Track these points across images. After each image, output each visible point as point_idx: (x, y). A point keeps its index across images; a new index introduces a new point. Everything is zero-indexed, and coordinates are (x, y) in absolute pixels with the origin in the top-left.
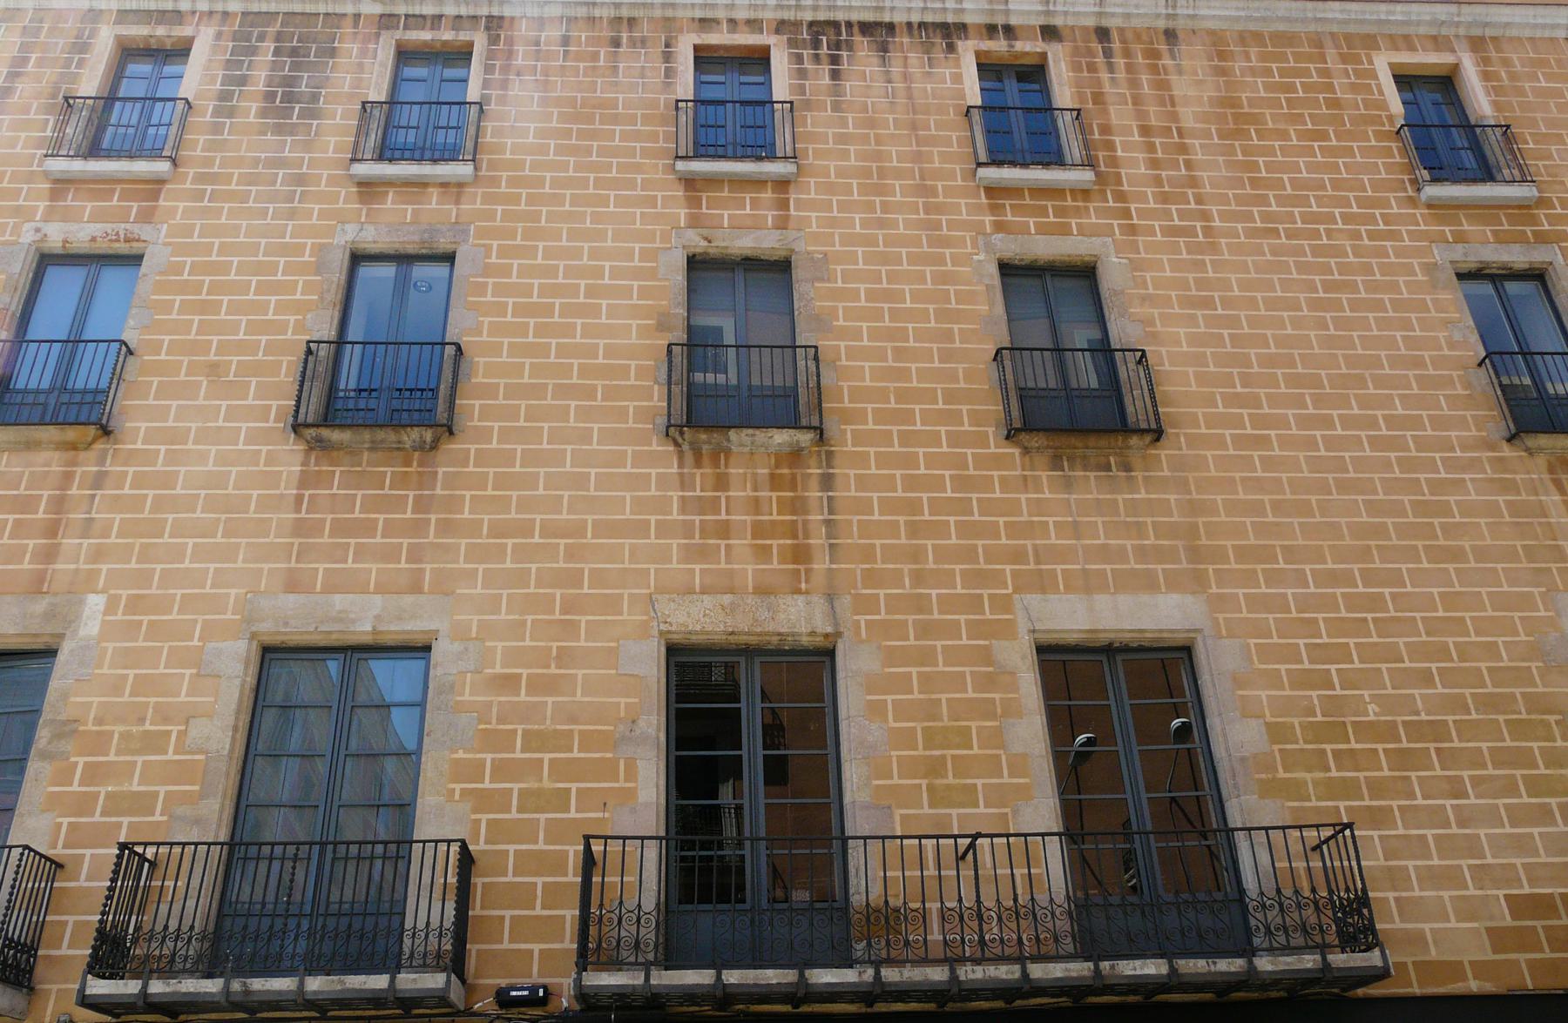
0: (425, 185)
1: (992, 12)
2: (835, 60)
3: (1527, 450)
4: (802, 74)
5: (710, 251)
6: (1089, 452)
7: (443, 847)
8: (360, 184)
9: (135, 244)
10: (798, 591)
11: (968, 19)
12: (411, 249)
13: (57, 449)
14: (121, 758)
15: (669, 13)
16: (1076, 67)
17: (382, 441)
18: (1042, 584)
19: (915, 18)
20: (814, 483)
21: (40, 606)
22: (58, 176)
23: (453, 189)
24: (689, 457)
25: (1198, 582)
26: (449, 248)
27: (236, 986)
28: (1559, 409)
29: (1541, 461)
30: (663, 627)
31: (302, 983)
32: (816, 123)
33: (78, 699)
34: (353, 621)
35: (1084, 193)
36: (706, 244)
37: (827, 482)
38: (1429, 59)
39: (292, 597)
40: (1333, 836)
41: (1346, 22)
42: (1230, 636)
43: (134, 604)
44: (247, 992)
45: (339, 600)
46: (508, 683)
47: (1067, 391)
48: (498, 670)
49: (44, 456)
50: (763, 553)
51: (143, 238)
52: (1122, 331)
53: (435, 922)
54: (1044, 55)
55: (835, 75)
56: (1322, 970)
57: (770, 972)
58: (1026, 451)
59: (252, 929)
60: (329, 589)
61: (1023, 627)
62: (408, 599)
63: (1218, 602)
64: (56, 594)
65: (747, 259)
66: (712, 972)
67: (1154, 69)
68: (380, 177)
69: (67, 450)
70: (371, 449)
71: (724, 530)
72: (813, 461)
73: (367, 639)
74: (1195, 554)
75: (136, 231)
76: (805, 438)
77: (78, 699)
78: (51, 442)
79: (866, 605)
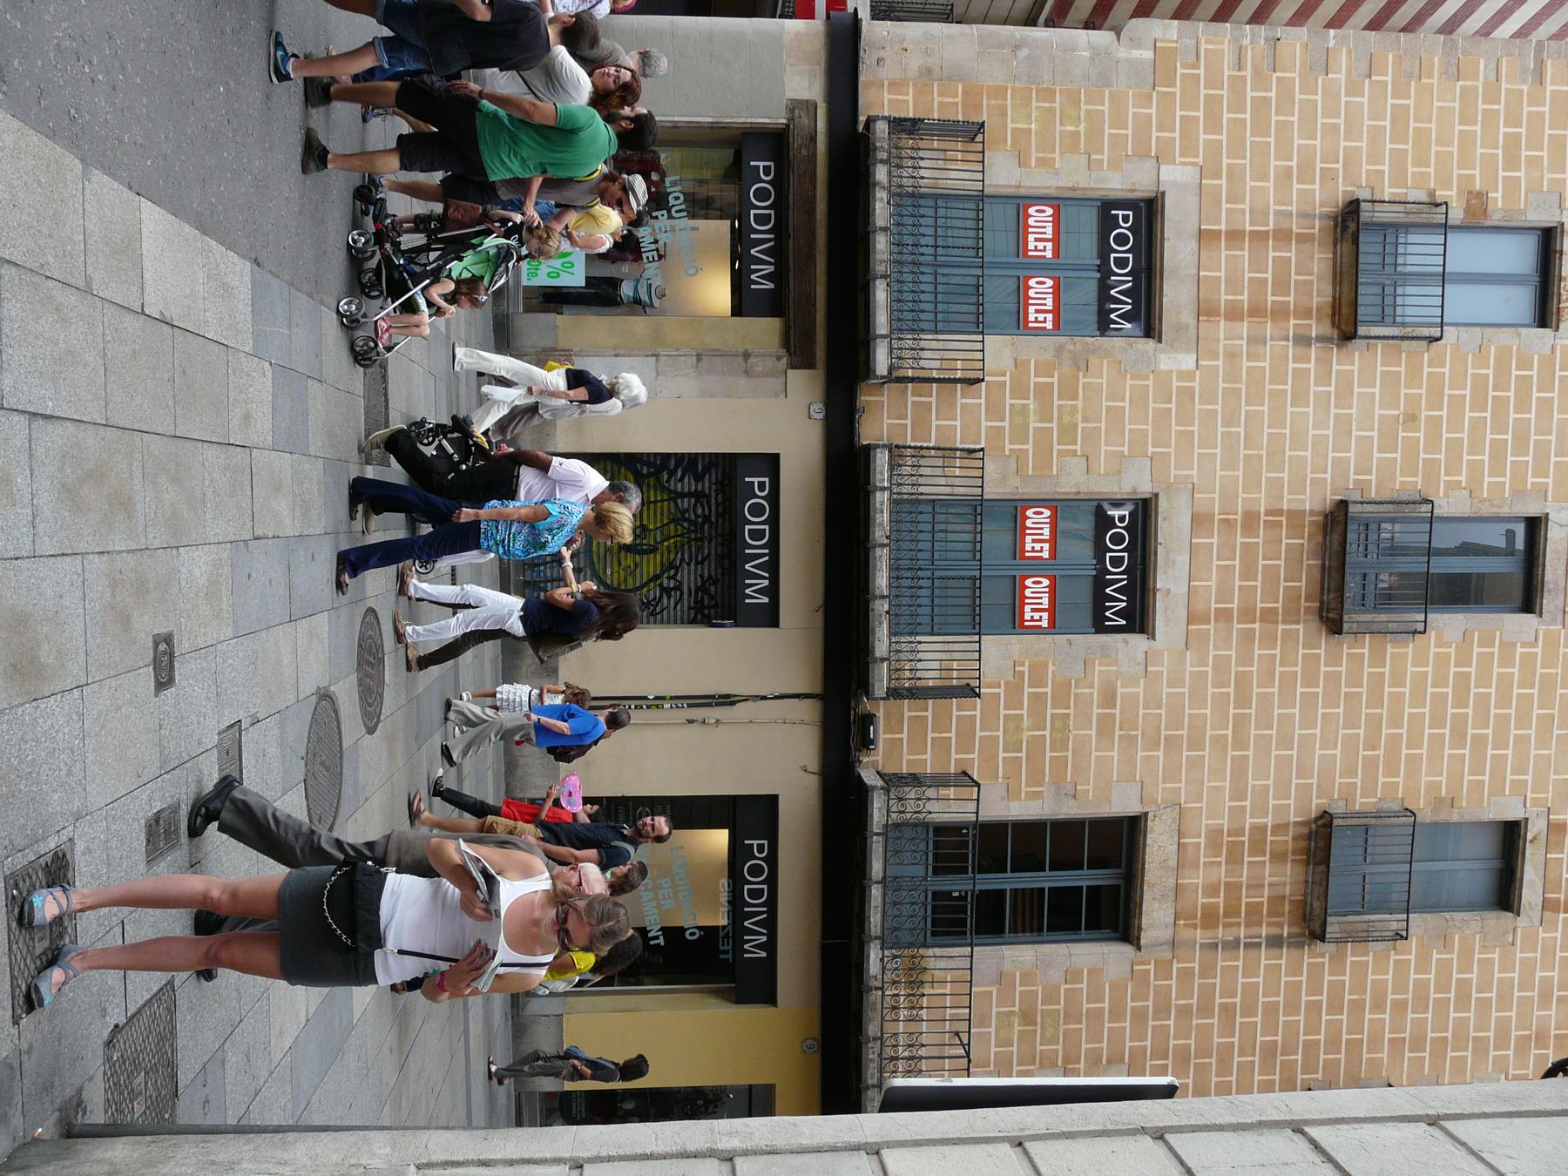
20: (1274, 931)
46: (1109, 698)
48: (1120, 690)
50: (1212, 890)
60: (1192, 548)
71: (1234, 859)
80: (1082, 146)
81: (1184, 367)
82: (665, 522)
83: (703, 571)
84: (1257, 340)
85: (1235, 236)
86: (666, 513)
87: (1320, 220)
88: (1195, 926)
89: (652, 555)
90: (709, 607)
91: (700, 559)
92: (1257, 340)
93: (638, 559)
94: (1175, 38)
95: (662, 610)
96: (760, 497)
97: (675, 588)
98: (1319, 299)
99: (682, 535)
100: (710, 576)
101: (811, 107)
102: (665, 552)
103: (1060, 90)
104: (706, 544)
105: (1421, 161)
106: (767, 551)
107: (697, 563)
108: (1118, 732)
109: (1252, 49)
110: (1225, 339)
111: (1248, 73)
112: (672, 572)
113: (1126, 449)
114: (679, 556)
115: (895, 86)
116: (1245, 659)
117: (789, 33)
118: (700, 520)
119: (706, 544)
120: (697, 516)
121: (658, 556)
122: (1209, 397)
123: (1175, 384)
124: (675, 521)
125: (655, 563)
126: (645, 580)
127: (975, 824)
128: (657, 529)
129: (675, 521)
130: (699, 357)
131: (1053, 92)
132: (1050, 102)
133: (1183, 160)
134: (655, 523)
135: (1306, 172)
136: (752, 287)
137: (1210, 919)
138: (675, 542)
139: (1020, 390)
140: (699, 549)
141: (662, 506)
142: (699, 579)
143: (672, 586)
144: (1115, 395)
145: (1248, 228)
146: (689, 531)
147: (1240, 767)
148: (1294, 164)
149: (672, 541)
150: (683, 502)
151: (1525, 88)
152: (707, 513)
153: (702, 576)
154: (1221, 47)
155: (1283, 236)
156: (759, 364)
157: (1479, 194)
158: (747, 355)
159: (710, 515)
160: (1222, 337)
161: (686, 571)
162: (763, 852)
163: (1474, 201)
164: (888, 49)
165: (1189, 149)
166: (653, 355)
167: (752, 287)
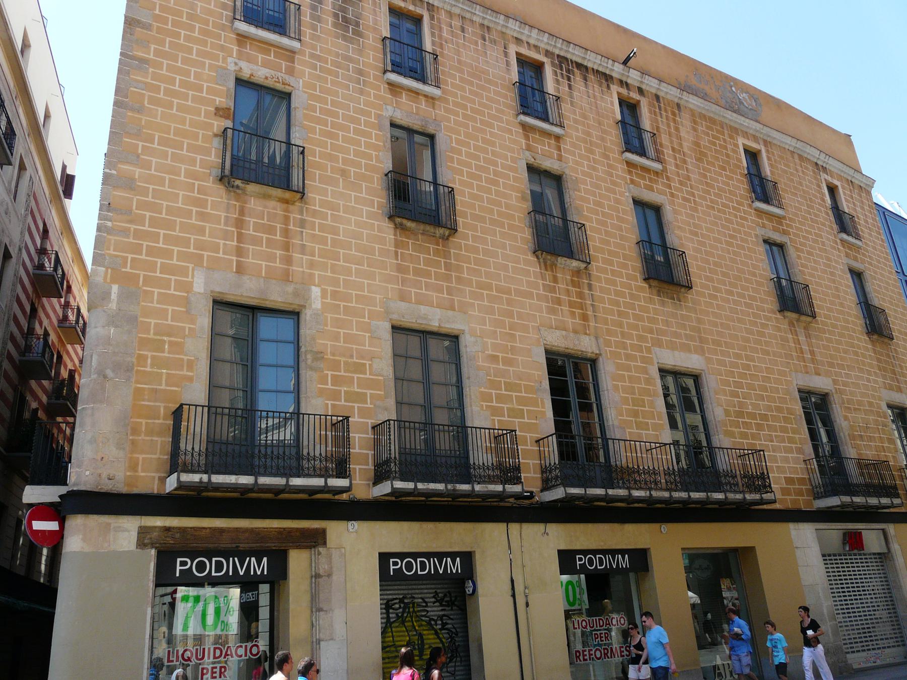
0: (418, 94)
1: (623, 74)
2: (569, 79)
3: (784, 316)
4: (557, 81)
5: (535, 164)
6: (669, 291)
7: (201, 408)
8: (238, 35)
9: (287, 87)
10: (586, 334)
11: (614, 75)
12: (416, 127)
13: (278, 201)
14: (347, 374)
15: (504, 30)
16: (650, 112)
17: (428, 231)
18: (658, 343)
19: (596, 67)
20: (586, 286)
21: (290, 288)
22: (239, 32)
23: (430, 99)
24: (543, 267)
25: (701, 351)
26: (433, 132)
27: (450, 487)
28: (266, 174)
29: (787, 320)
30: (545, 342)
31: (287, 481)
32: (565, 107)
33: (321, 342)
34: (430, 320)
35: (656, 173)
36: (533, 160)
37: (590, 287)
38: (754, 145)
39: (403, 304)
40: (341, 421)
41: (731, 120)
42: (712, 374)
43: (335, 294)
44: (454, 490)
45: (423, 309)
46: (494, 359)
47: (238, 156)
48: (490, 352)
49: (272, 203)
50: (573, 314)
51: (292, 84)
52: (297, 138)
53: (197, 449)
54: (639, 102)
55: (570, 87)
56: (324, 486)
57: (620, 491)
58: (650, 286)
59: (275, 453)
60: (419, 302)
61: (655, 361)
62: (450, 313)
63: (708, 360)
64: (296, 283)
65: (546, 171)
66: (723, 494)
67: (674, 121)
68: (399, 83)
69: (283, 203)
70: (422, 234)
71: (559, 302)
72: (584, 276)
73: (435, 329)
74: (702, 340)
75: (287, 79)
76: (583, 265)
77: (321, 342)
78: (276, 197)
79: (608, 343)
80: (179, 340)
81: (319, 294)
82: (404, 629)
83: (431, 602)
84: (303, 249)
85: (240, 252)
86: (399, 629)
87: (230, 200)
88: (589, 325)
89: (424, 637)
90: (451, 597)
91: (424, 604)
92: (303, 249)
93: (426, 646)
94: (104, 269)
95: (454, 628)
96: (402, 564)
97: (442, 620)
98: (278, 209)
99: (411, 617)
100: (434, 597)
101: (143, 532)
102: (422, 628)
103: (139, 350)
104: (416, 600)
105: (195, 137)
106: (231, 559)
107: (427, 606)
108: (510, 356)
109: (115, 221)
110: (302, 267)
111: (133, 227)
112: (433, 622)
113: (367, 335)
114: (423, 618)
115: (133, 466)
116: (469, 283)
117: (82, 548)
118: (402, 605)
119: (416, 600)
120: (400, 607)
121: (425, 632)
122: (336, 282)
123: (329, 301)
124: (403, 623)
125: (428, 634)
126: (438, 641)
127: (559, 437)
128: (409, 635)
129: (403, 623)
130: (320, 610)
131: (139, 356)
132: (147, 358)
133: (190, 276)
134: (404, 636)
135: (202, 203)
136: (265, 573)
137: (585, 318)
138: (416, 621)
139: (335, 396)
140: (419, 605)
141: (396, 632)
142: (436, 604)
143: (440, 622)
144: (336, 337)
145: (235, 243)
146: (409, 612)
147: (519, 293)
148: (194, 209)
149: (415, 624)
150: (393, 618)
151: (151, 70)
152: (397, 601)
153: (434, 603)
154: (113, 242)
155: (240, 223)
156: (323, 568)
157: (217, 109)
158: (317, 576)
159: (399, 599)
160: (301, 269)
161: (432, 613)
162: (397, 562)
163: (221, 113)
164: (99, 471)
165: (183, 271)
166: (319, 644)
167: (265, 573)
